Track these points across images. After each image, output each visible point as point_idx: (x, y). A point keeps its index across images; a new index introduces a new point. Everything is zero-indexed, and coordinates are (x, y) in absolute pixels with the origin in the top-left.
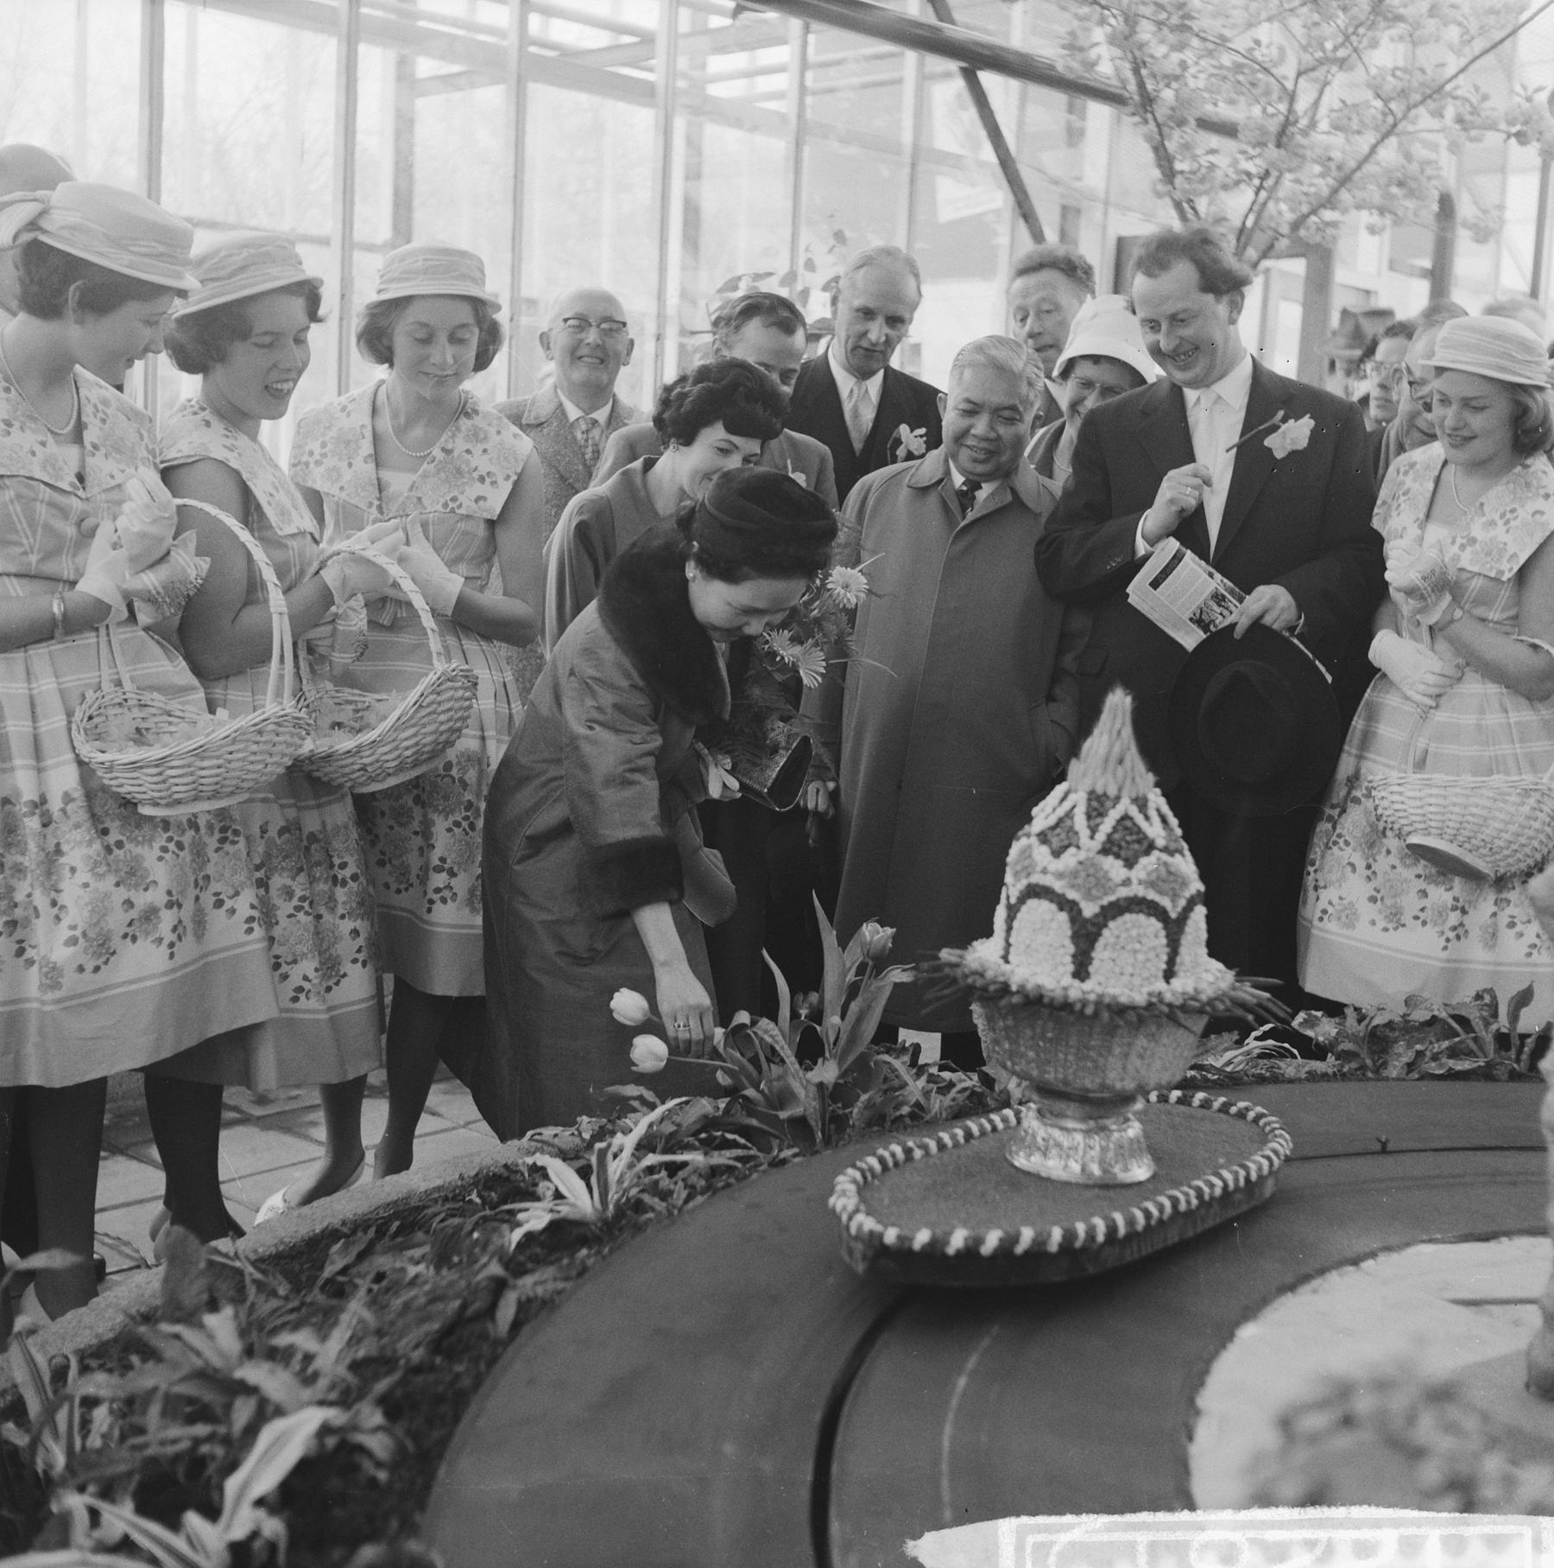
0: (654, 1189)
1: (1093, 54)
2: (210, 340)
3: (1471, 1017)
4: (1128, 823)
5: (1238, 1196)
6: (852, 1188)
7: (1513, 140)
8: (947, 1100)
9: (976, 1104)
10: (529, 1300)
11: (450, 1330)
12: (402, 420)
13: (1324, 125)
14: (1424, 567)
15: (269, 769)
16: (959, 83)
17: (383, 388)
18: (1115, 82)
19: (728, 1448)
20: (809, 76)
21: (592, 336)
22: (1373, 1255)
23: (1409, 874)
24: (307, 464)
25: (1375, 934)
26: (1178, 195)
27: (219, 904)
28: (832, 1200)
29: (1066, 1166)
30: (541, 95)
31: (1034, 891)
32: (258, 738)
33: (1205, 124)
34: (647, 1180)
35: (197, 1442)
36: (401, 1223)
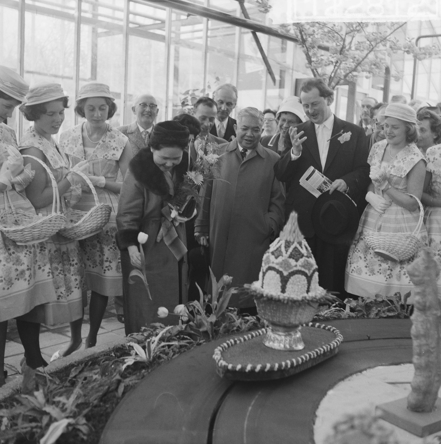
0: (164, 352)
1: (289, 28)
2: (34, 113)
3: (394, 300)
4: (296, 249)
5: (328, 353)
6: (219, 352)
7: (406, 53)
8: (247, 325)
9: (255, 327)
10: (127, 386)
11: (105, 395)
12: (90, 133)
13: (353, 48)
14: (380, 173)
15: (54, 231)
16: (250, 35)
17: (85, 124)
18: (295, 36)
19: (184, 429)
20: (209, 32)
21: (148, 109)
22: (365, 369)
23: (376, 260)
24: (64, 147)
25: (367, 276)
26: (313, 68)
27: (40, 268)
28: (214, 356)
29: (279, 346)
30: (133, 39)
31: (270, 268)
32: (50, 223)
33: (320, 47)
34: (162, 349)
35: (32, 428)
36: (92, 362)
